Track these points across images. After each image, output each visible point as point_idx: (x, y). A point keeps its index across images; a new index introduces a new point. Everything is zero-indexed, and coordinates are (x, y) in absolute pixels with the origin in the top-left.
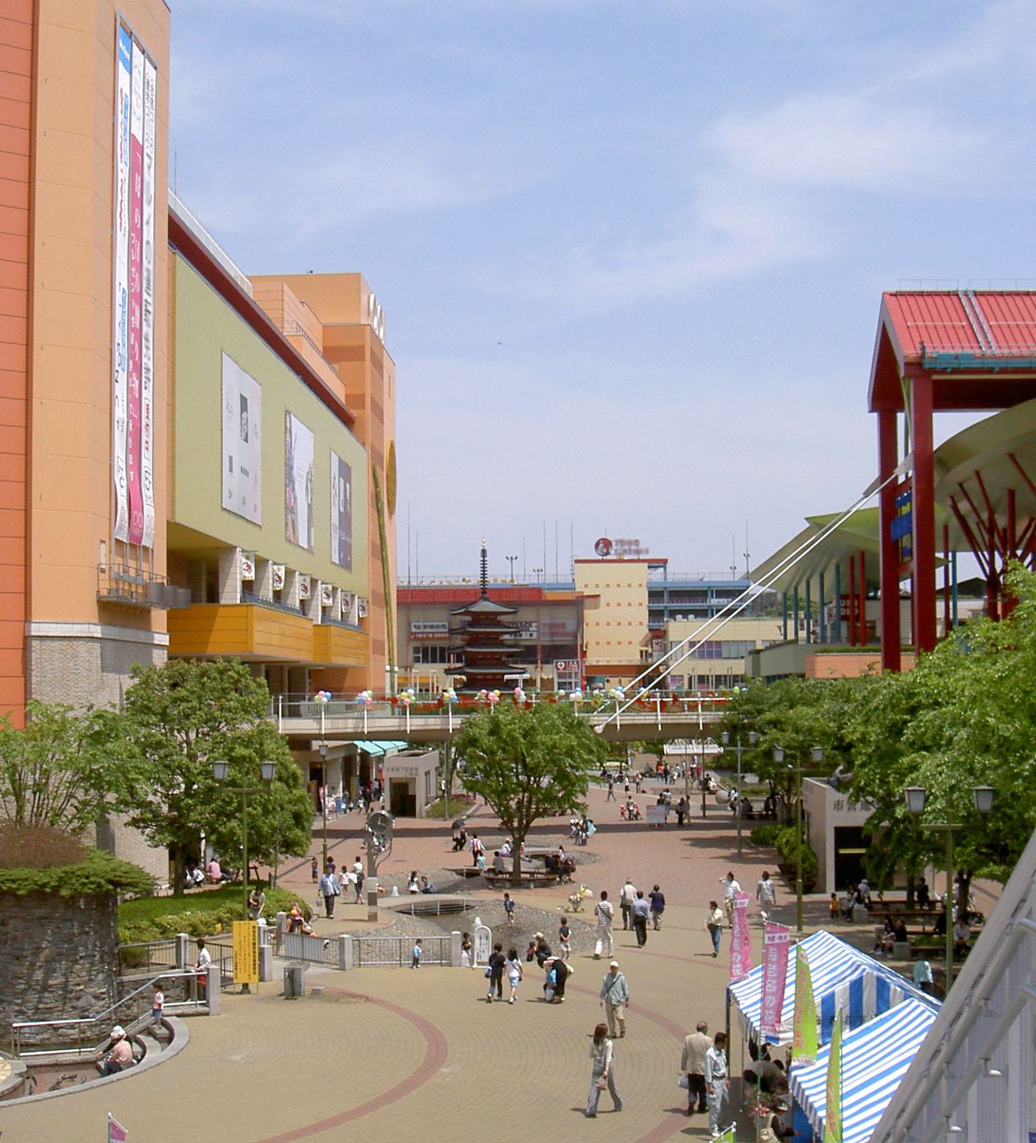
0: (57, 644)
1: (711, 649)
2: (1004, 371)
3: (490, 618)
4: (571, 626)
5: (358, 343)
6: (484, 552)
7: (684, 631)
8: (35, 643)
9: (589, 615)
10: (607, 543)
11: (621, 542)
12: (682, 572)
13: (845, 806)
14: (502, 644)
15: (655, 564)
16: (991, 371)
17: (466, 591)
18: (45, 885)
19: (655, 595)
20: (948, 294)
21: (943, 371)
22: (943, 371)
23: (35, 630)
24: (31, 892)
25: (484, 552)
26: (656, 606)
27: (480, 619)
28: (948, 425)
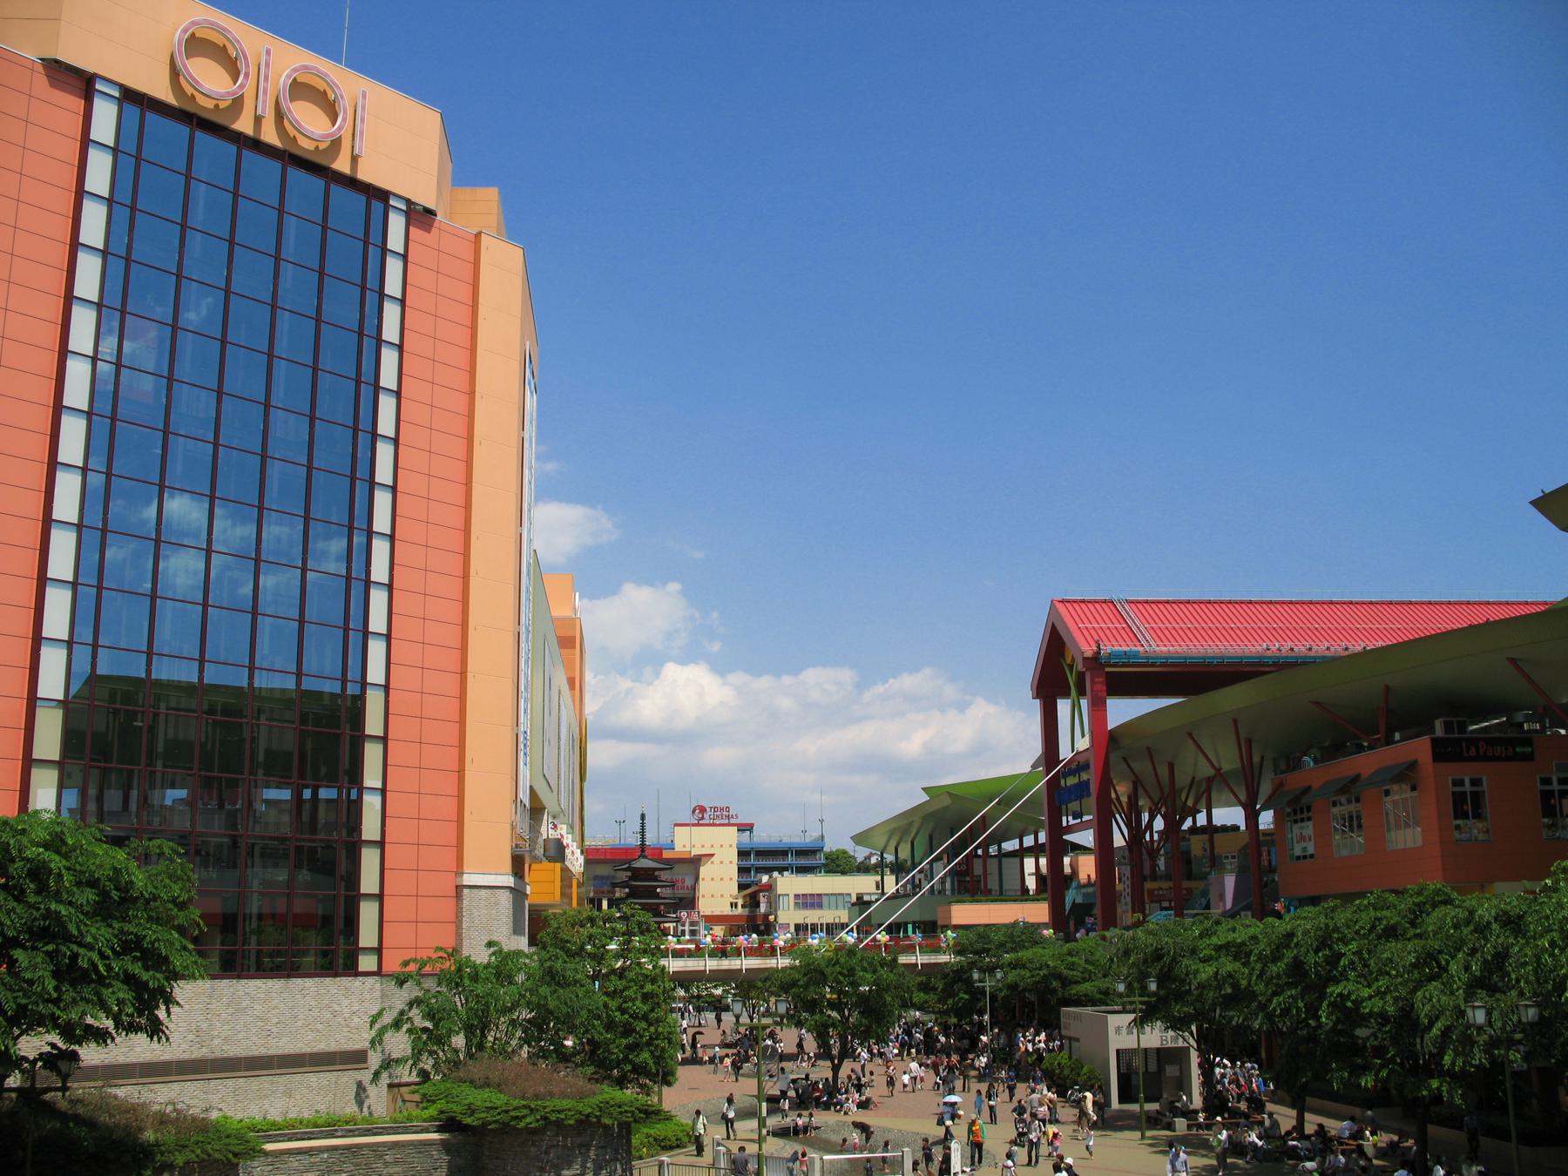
0: (483, 892)
1: (809, 901)
2: (1162, 665)
3: (649, 874)
4: (689, 882)
5: (570, 634)
6: (643, 817)
7: (789, 884)
8: (466, 891)
9: (705, 871)
10: (703, 810)
11: (715, 809)
12: (765, 835)
13: (1124, 1031)
14: (657, 896)
15: (746, 828)
16: (1153, 665)
17: (627, 850)
18: (588, 1116)
19: (743, 854)
20: (1105, 602)
21: (1115, 665)
22: (1115, 665)
23: (468, 879)
24: (579, 1122)
25: (643, 817)
26: (744, 863)
27: (638, 874)
28: (1122, 711)
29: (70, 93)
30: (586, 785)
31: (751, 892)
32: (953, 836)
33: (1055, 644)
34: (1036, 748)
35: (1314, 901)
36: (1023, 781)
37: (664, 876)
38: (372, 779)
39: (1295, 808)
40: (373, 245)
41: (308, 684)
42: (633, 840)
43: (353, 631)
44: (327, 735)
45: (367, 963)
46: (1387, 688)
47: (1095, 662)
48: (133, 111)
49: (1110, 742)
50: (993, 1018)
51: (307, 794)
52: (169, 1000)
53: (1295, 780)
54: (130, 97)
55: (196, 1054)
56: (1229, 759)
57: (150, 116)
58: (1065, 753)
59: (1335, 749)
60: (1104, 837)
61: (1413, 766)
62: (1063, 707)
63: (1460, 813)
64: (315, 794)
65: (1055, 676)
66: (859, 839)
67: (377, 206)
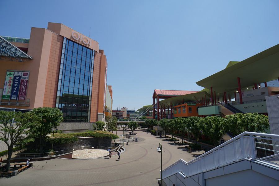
23: (99, 114)
28: (160, 100)
29: (202, 91)
30: (112, 105)
31: (128, 115)
32: (145, 110)
33: (155, 93)
34: (153, 103)
35: (177, 117)
36: (151, 106)
37: (120, 113)
38: (90, 104)
39: (175, 109)
40: (91, 54)
41: (74, 94)
42: (117, 110)
43: (88, 90)
44: (85, 100)
45: (89, 121)
46: (183, 99)
47: (158, 95)
48: (68, 41)
49: (159, 102)
50: (148, 127)
51: (85, 105)
52: (59, 125)
53: (175, 107)
54: (67, 39)
55: (72, 129)
56: (170, 105)
57: (69, 41)
58: (155, 103)
59: (179, 104)
60: (172, 110)
61: (185, 106)
62: (155, 99)
63: (189, 110)
64: (86, 105)
65: (155, 96)
66: (137, 110)
67: (92, 51)
